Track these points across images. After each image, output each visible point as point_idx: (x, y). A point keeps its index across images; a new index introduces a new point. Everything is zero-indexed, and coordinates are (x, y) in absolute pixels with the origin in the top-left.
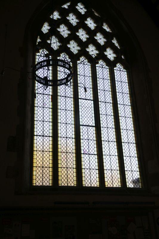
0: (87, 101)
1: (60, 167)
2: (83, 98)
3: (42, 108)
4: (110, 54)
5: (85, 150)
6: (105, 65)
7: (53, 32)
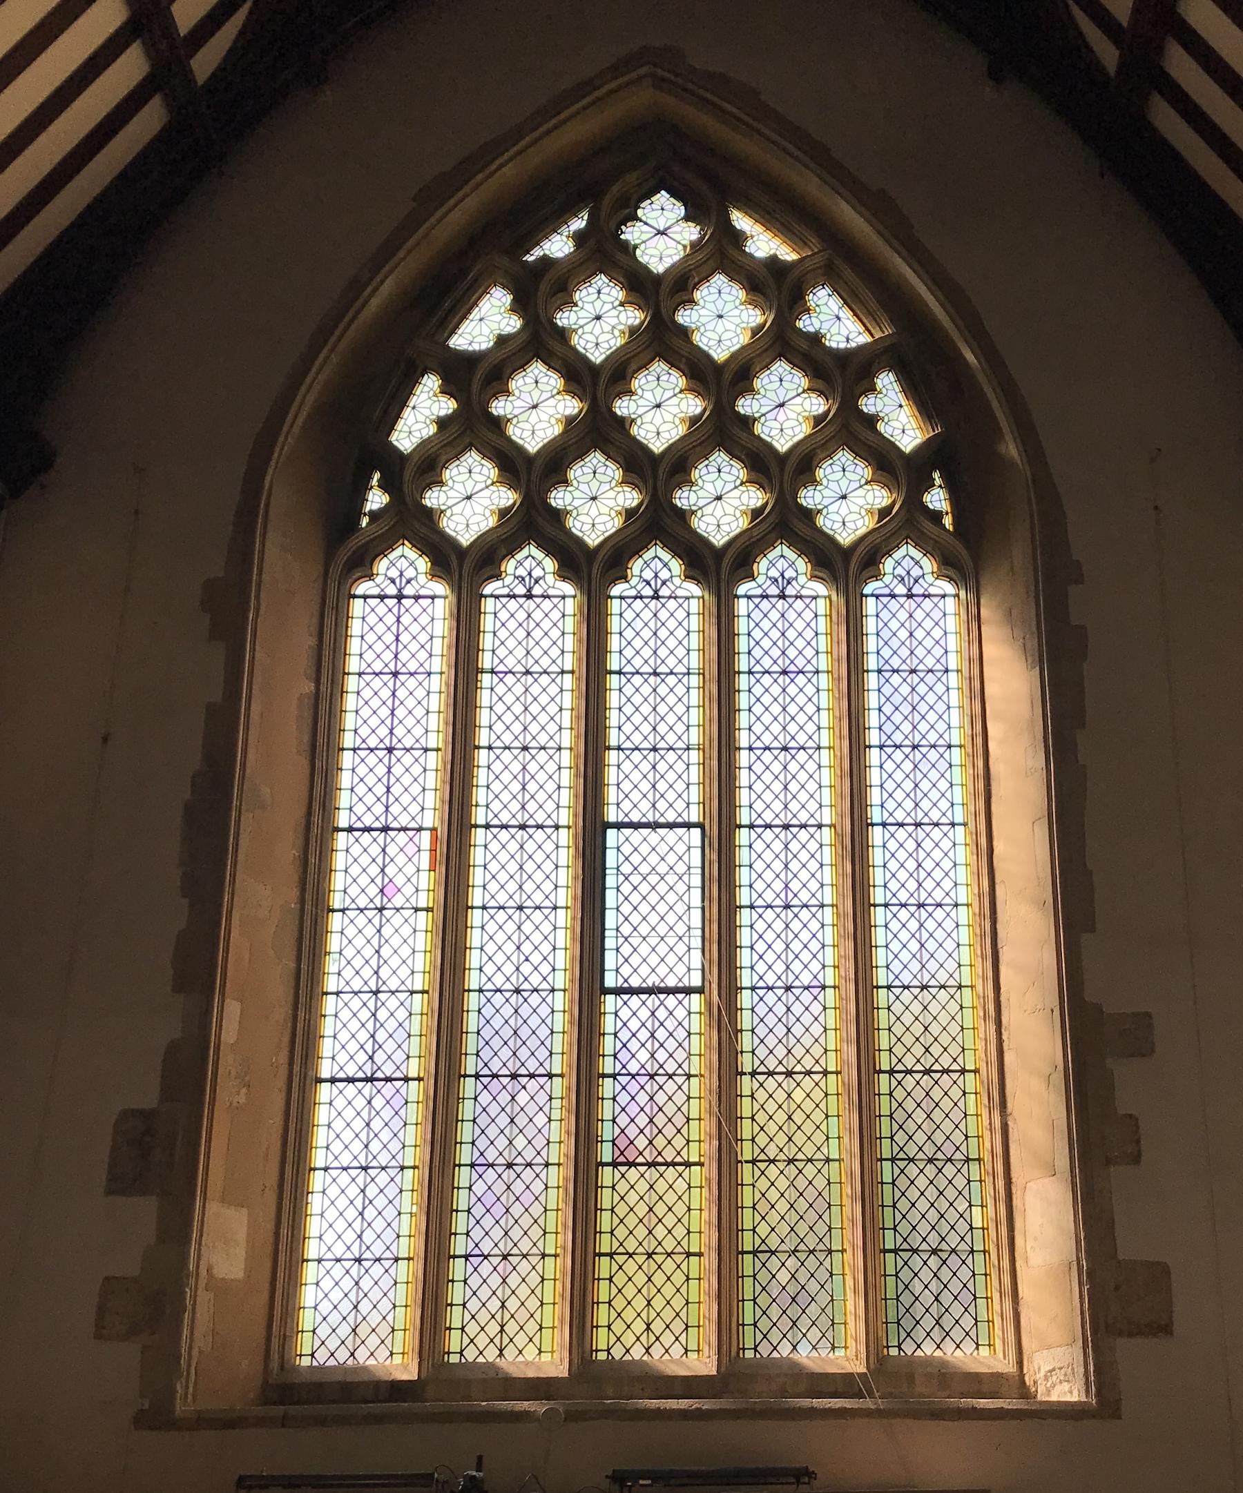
0: (662, 831)
1: (336, 907)
2: (635, 820)
3: (381, 753)
4: (847, 500)
5: (622, 1142)
6: (802, 579)
7: (473, 428)
